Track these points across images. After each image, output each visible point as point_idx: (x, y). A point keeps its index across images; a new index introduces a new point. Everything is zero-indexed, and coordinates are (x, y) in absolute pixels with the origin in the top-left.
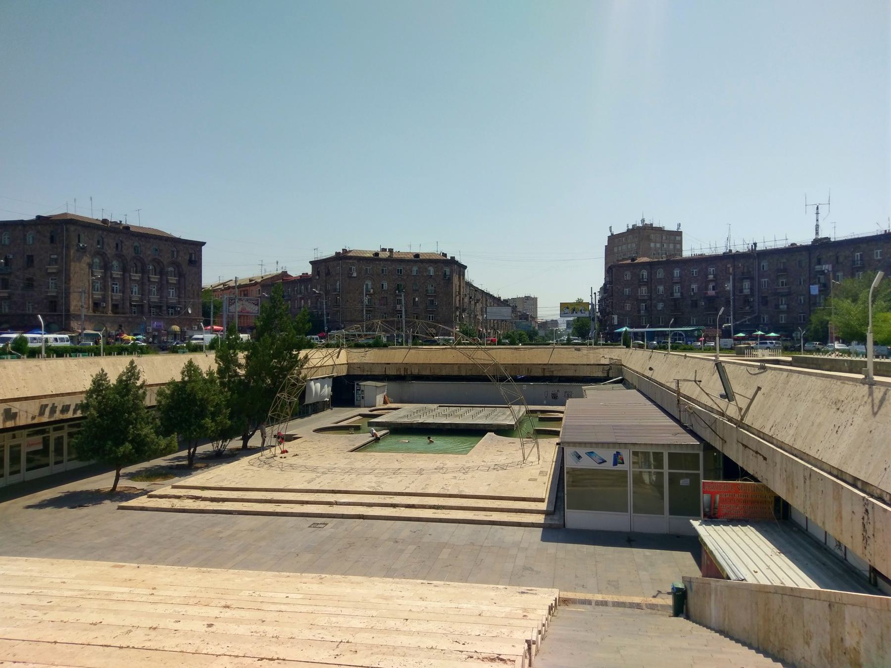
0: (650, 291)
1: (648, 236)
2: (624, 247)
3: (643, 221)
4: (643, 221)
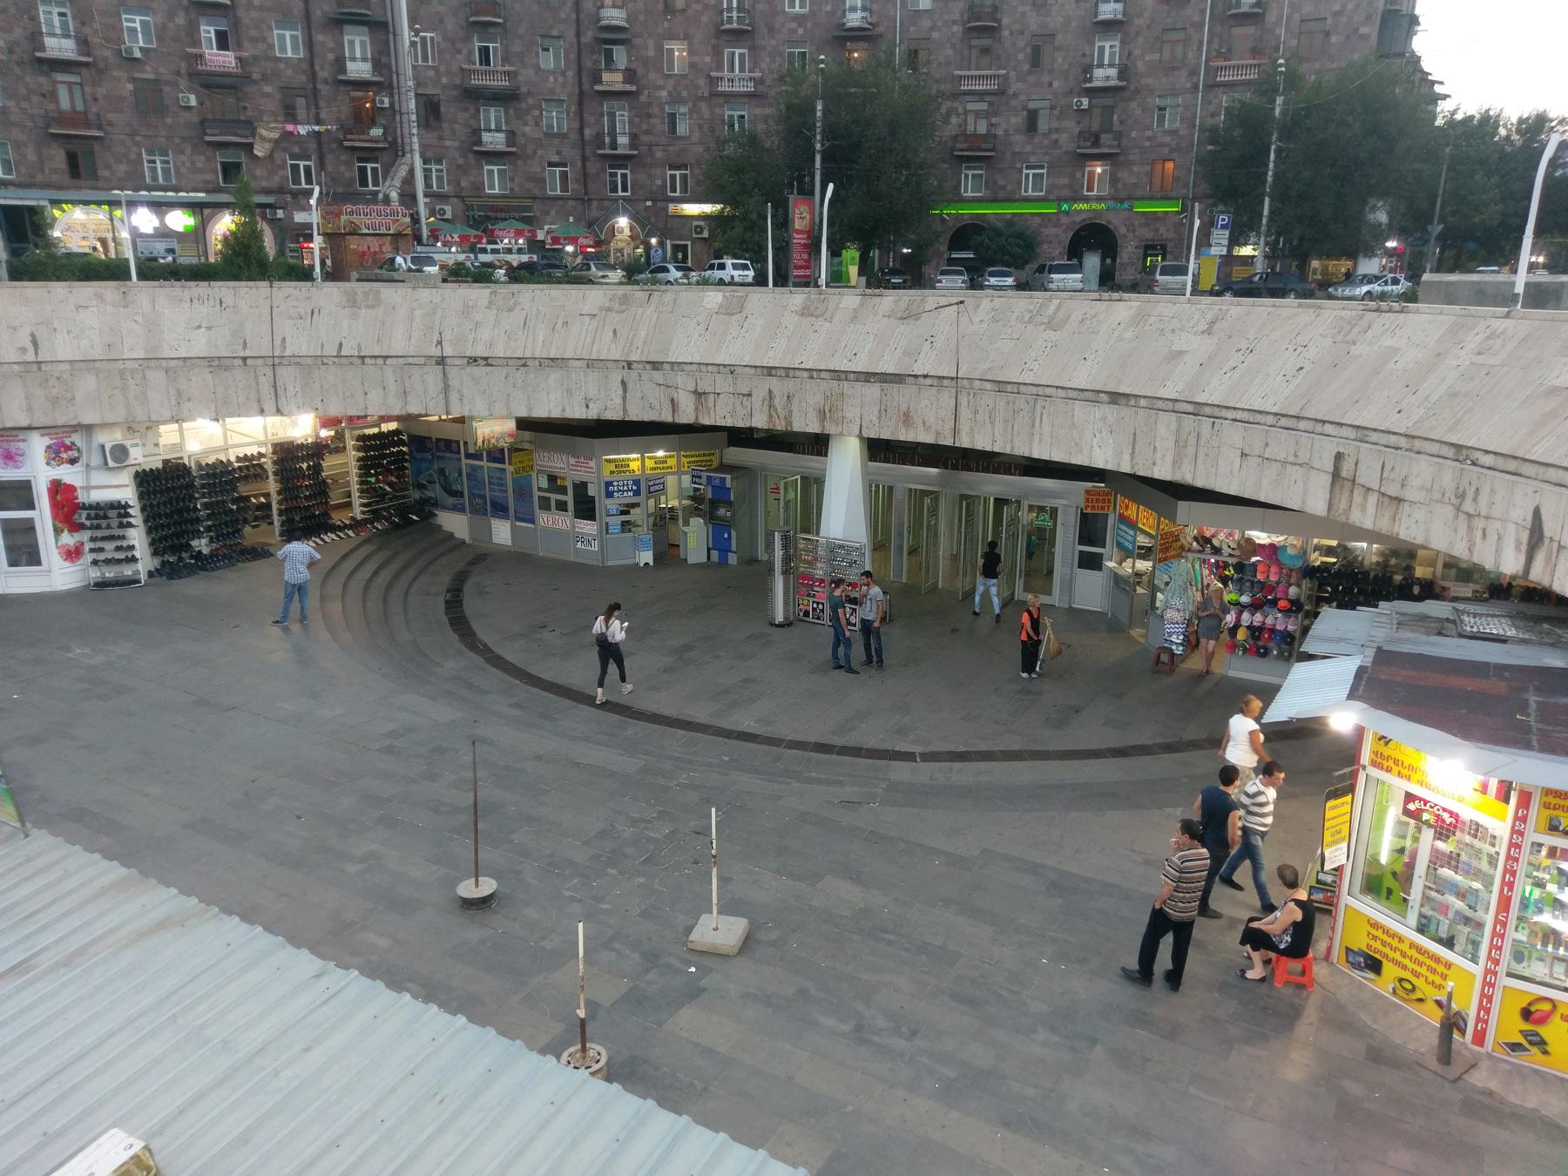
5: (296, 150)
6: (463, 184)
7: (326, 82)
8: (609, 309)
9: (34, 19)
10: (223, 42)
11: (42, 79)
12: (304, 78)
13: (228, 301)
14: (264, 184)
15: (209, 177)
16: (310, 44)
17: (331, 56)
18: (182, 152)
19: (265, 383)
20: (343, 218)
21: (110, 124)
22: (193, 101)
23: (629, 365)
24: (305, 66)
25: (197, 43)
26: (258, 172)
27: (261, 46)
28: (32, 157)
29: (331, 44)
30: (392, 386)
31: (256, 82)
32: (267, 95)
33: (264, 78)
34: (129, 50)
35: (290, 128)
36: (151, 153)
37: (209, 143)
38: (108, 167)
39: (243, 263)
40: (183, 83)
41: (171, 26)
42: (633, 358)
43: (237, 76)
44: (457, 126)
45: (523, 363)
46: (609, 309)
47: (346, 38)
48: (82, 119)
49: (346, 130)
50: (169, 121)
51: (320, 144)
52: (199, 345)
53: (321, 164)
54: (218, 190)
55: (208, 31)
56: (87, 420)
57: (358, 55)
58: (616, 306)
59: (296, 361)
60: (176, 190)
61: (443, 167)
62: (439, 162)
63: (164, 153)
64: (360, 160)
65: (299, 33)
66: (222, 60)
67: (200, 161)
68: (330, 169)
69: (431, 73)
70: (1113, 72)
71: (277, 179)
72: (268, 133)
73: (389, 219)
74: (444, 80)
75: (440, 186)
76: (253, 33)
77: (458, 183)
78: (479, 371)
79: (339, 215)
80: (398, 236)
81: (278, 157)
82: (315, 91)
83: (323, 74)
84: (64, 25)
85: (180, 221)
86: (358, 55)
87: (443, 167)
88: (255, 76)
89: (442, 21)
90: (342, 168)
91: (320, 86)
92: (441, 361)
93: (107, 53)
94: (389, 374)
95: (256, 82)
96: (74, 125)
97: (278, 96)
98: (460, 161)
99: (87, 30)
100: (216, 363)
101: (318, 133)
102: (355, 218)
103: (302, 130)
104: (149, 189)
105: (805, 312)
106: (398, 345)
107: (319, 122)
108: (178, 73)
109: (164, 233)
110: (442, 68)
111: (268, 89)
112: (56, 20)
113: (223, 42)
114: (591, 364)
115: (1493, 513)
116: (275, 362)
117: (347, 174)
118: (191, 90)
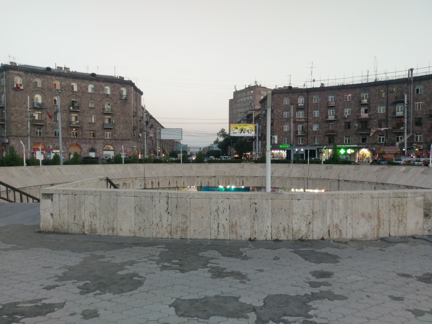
0: (307, 114)
1: (260, 92)
2: (244, 99)
3: (256, 82)
4: (256, 82)
5: (380, 134)
6: (428, 139)
7: (390, 117)
8: (378, 171)
9: (327, 113)
10: (366, 111)
11: (327, 124)
12: (384, 117)
13: (305, 167)
14: (371, 142)
15: (358, 141)
16: (387, 109)
17: (392, 111)
18: (353, 136)
19: (306, 183)
20: (381, 150)
21: (339, 132)
22: (357, 125)
23: (377, 183)
24: (385, 114)
25: (360, 112)
26: (370, 140)
27: (375, 111)
28: (322, 140)
29: (392, 109)
30: (328, 185)
31: (372, 119)
32: (375, 122)
33: (374, 118)
34: (345, 116)
35: (379, 129)
36: (346, 137)
37: (359, 134)
38: (337, 140)
39: (300, 159)
40: (355, 122)
41: (355, 110)
42: (379, 182)
43: (368, 119)
44: (427, 125)
45: (355, 182)
46: (378, 171)
47: (397, 107)
48: (333, 131)
49: (394, 128)
50: (351, 130)
51: (387, 132)
52: (297, 175)
53: (387, 137)
54: (360, 144)
55: (363, 110)
56: (277, 187)
57: (400, 110)
58: (380, 170)
59: (313, 179)
60: (350, 145)
61: (422, 135)
62: (421, 134)
63: (349, 137)
64: (397, 135)
65: (384, 107)
66: (364, 115)
67: (357, 138)
68: (389, 138)
69: (421, 112)
70: (333, 117)
71: (375, 141)
72: (373, 131)
73: (394, 150)
74: (424, 113)
75: (420, 140)
76: (373, 109)
77: (426, 139)
78: (346, 183)
79: (380, 149)
80: (396, 154)
81: (376, 136)
82: (387, 120)
83: (390, 115)
84: (333, 113)
85: (349, 151)
86: (400, 110)
87: (422, 135)
88: (372, 118)
89: (425, 99)
90: (392, 138)
91: (389, 119)
92: (339, 181)
93: (340, 117)
94: (328, 182)
95: (372, 119)
96: (332, 133)
97: (378, 122)
98: (427, 134)
99: (337, 114)
100: (299, 179)
101: (387, 130)
102: (384, 150)
103: (382, 129)
104: (344, 145)
105: (423, 173)
106: (331, 177)
107: (387, 127)
108: (355, 120)
109: (346, 154)
110: (424, 110)
111: (375, 121)
112: (332, 112)
113: (366, 111)
114: (369, 183)
115: (179, 186)
116: (308, 179)
117: (393, 139)
118: (357, 123)
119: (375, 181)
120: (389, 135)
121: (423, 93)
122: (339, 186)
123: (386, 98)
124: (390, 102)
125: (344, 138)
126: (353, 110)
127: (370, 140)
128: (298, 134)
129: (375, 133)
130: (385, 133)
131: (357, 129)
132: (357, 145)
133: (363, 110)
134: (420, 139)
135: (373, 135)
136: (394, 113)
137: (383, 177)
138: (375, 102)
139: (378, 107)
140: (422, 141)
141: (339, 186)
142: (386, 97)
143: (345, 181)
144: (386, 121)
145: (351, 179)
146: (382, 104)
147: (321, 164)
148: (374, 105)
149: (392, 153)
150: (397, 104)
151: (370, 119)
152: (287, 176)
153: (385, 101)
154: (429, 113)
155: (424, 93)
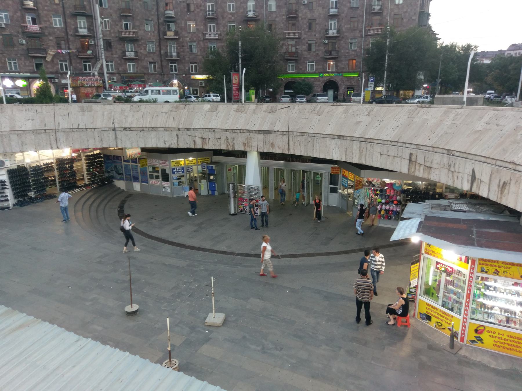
5: (62, 59)
6: (120, 69)
7: (71, 35)
8: (171, 111)
14: (51, 70)
15: (31, 68)
16: (65, 23)
17: (73, 27)
18: (21, 60)
20: (79, 82)
22: (24, 42)
23: (179, 129)
24: (64, 30)
25: (25, 22)
26: (49, 66)
27: (48, 23)
29: (73, 23)
30: (97, 138)
31: (47, 36)
36: (9, 60)
40: (20, 36)
41: (15, 16)
42: (180, 127)
43: (40, 33)
45: (143, 129)
46: (171, 111)
49: (79, 52)
51: (70, 56)
52: (29, 126)
53: (71, 63)
54: (34, 73)
55: (29, 18)
58: (174, 109)
59: (64, 130)
60: (19, 73)
62: (111, 62)
64: (84, 62)
67: (27, 63)
68: (74, 65)
69: (108, 33)
71: (55, 68)
74: (113, 35)
75: (112, 70)
77: (118, 69)
78: (128, 132)
79: (77, 81)
80: (98, 87)
81: (55, 60)
82: (68, 39)
83: (71, 33)
86: (82, 26)
88: (46, 34)
89: (111, 15)
90: (78, 65)
91: (69, 37)
92: (114, 129)
94: (96, 134)
95: (47, 36)
100: (35, 132)
101: (69, 53)
102: (83, 81)
104: (9, 72)
105: (238, 111)
107: (69, 49)
110: (112, 31)
114: (166, 129)
119: (174, 126)
120: (73, 61)
121: (107, 7)
122: (116, 138)
123: (61, 5)
124: (68, 12)
125: (5, 61)
126: (13, 16)
127: (49, 66)
128: (328, 34)
129: (54, 56)
130: (68, 57)
131: (25, 48)
132: (30, 73)
133: (29, 18)
134: (112, 68)
135: (52, 60)
136: (76, 30)
137: (183, 119)
138: (46, 8)
139: (51, 17)
140: (114, 71)
141: (116, 138)
142: (61, 3)
143: (125, 129)
144: (67, 41)
145: (134, 126)
146: (57, 15)
147: (69, 103)
148: (45, 12)
149: (93, 85)
150: (78, 17)
151: (43, 34)
152: (8, 129)
153: (61, 10)
154: (117, 35)
155: (109, 6)
